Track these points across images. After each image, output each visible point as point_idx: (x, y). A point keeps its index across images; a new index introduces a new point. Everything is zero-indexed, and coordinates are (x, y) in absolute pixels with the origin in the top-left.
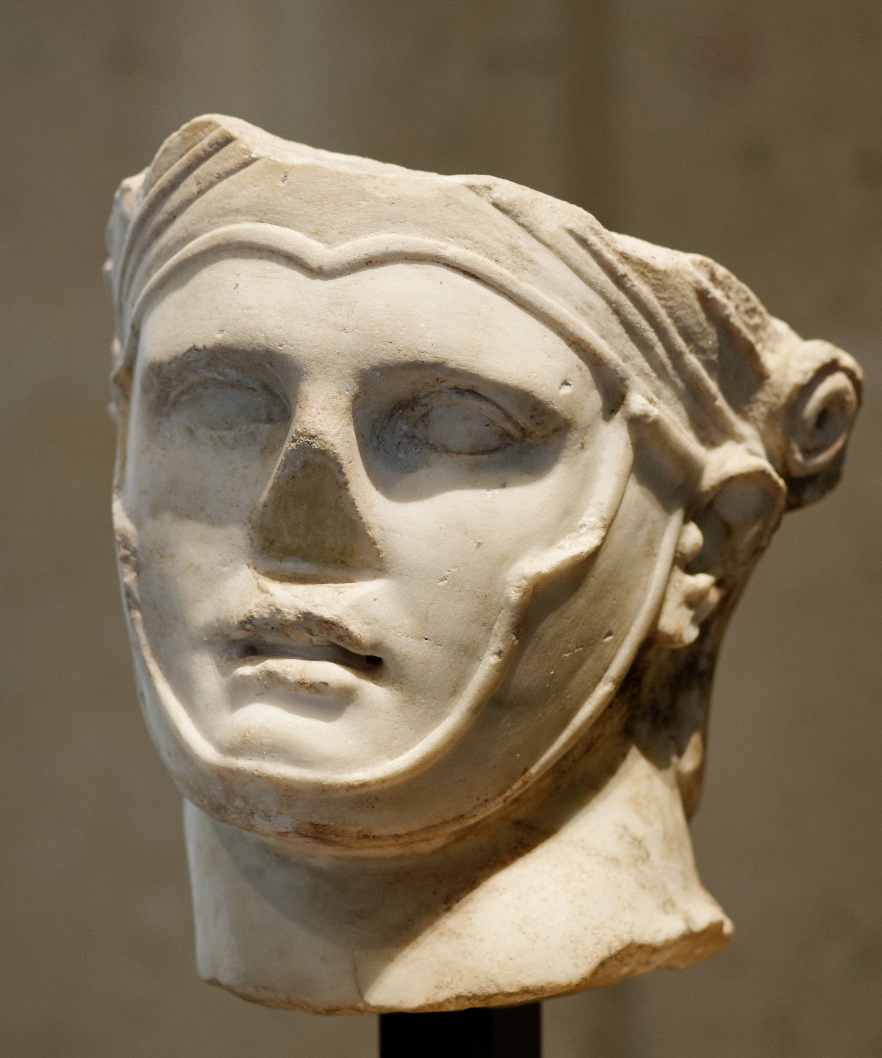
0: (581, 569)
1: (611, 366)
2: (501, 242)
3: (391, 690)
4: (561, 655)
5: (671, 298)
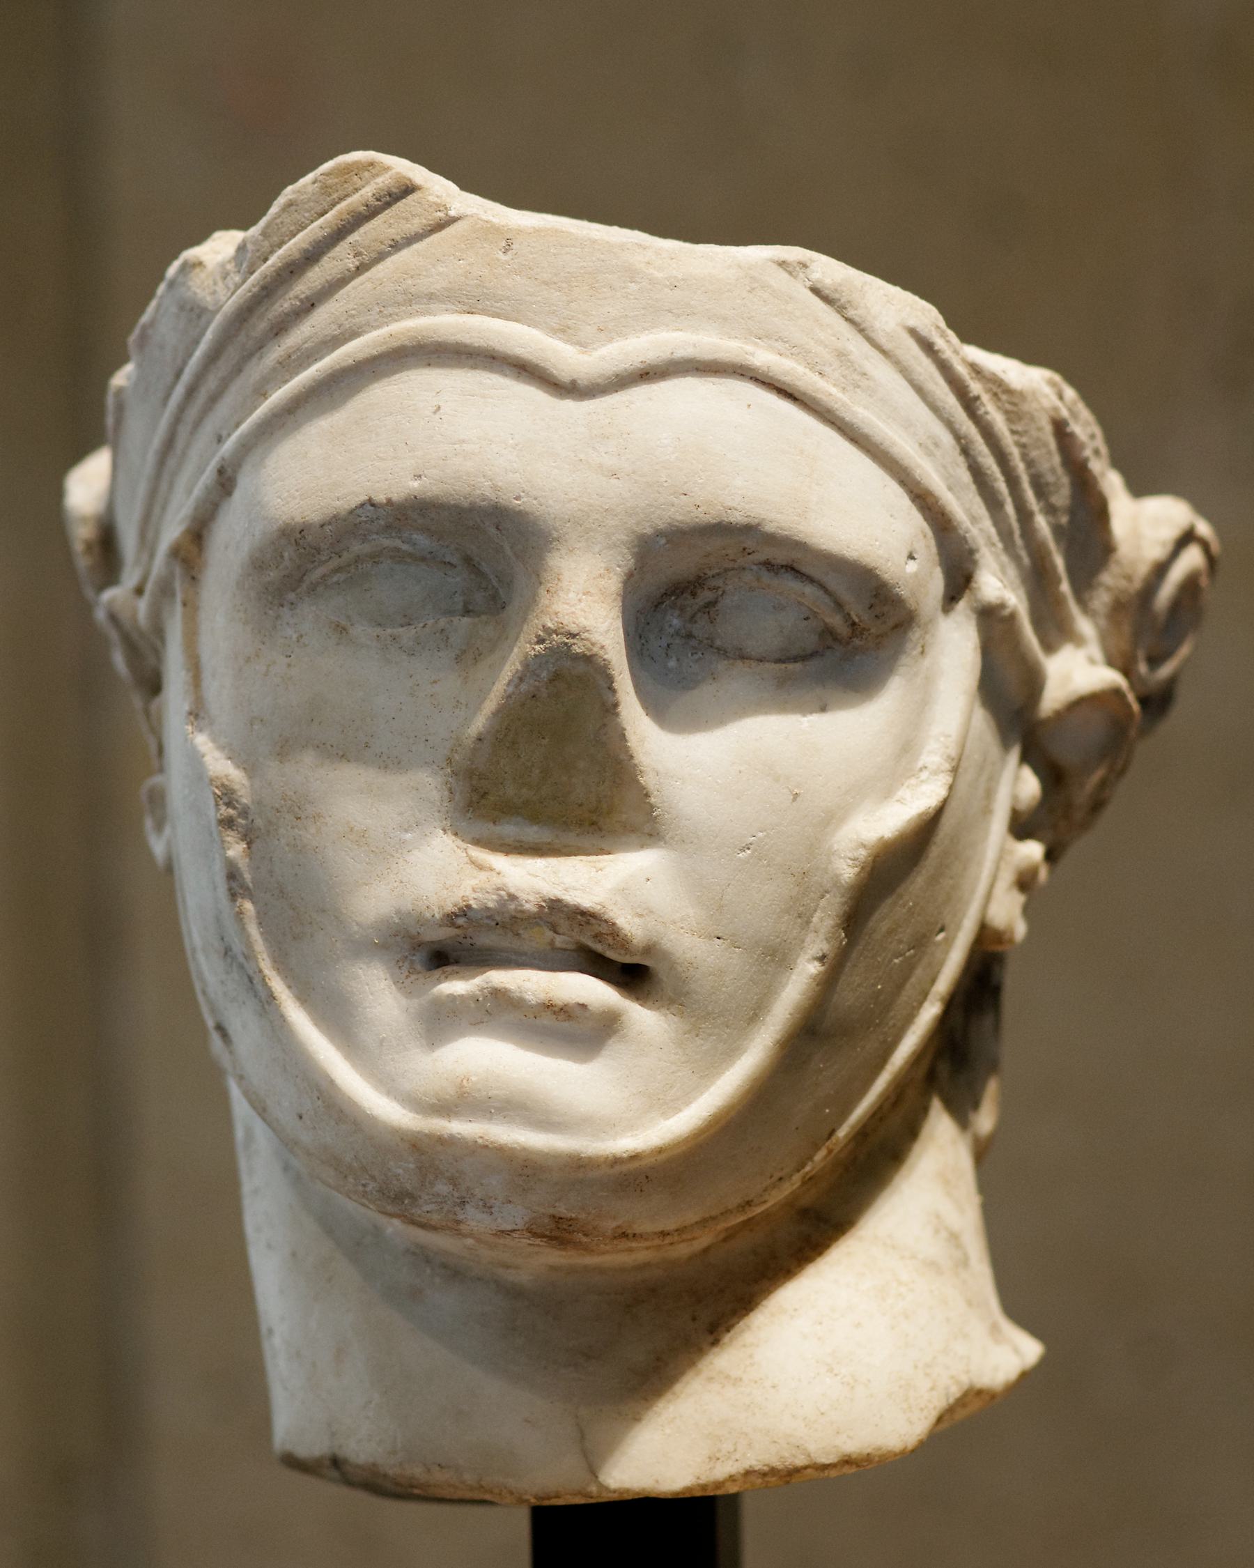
0: (925, 832)
1: (961, 532)
2: (826, 346)
3: (665, 1015)
4: (890, 961)
5: (1026, 432)
